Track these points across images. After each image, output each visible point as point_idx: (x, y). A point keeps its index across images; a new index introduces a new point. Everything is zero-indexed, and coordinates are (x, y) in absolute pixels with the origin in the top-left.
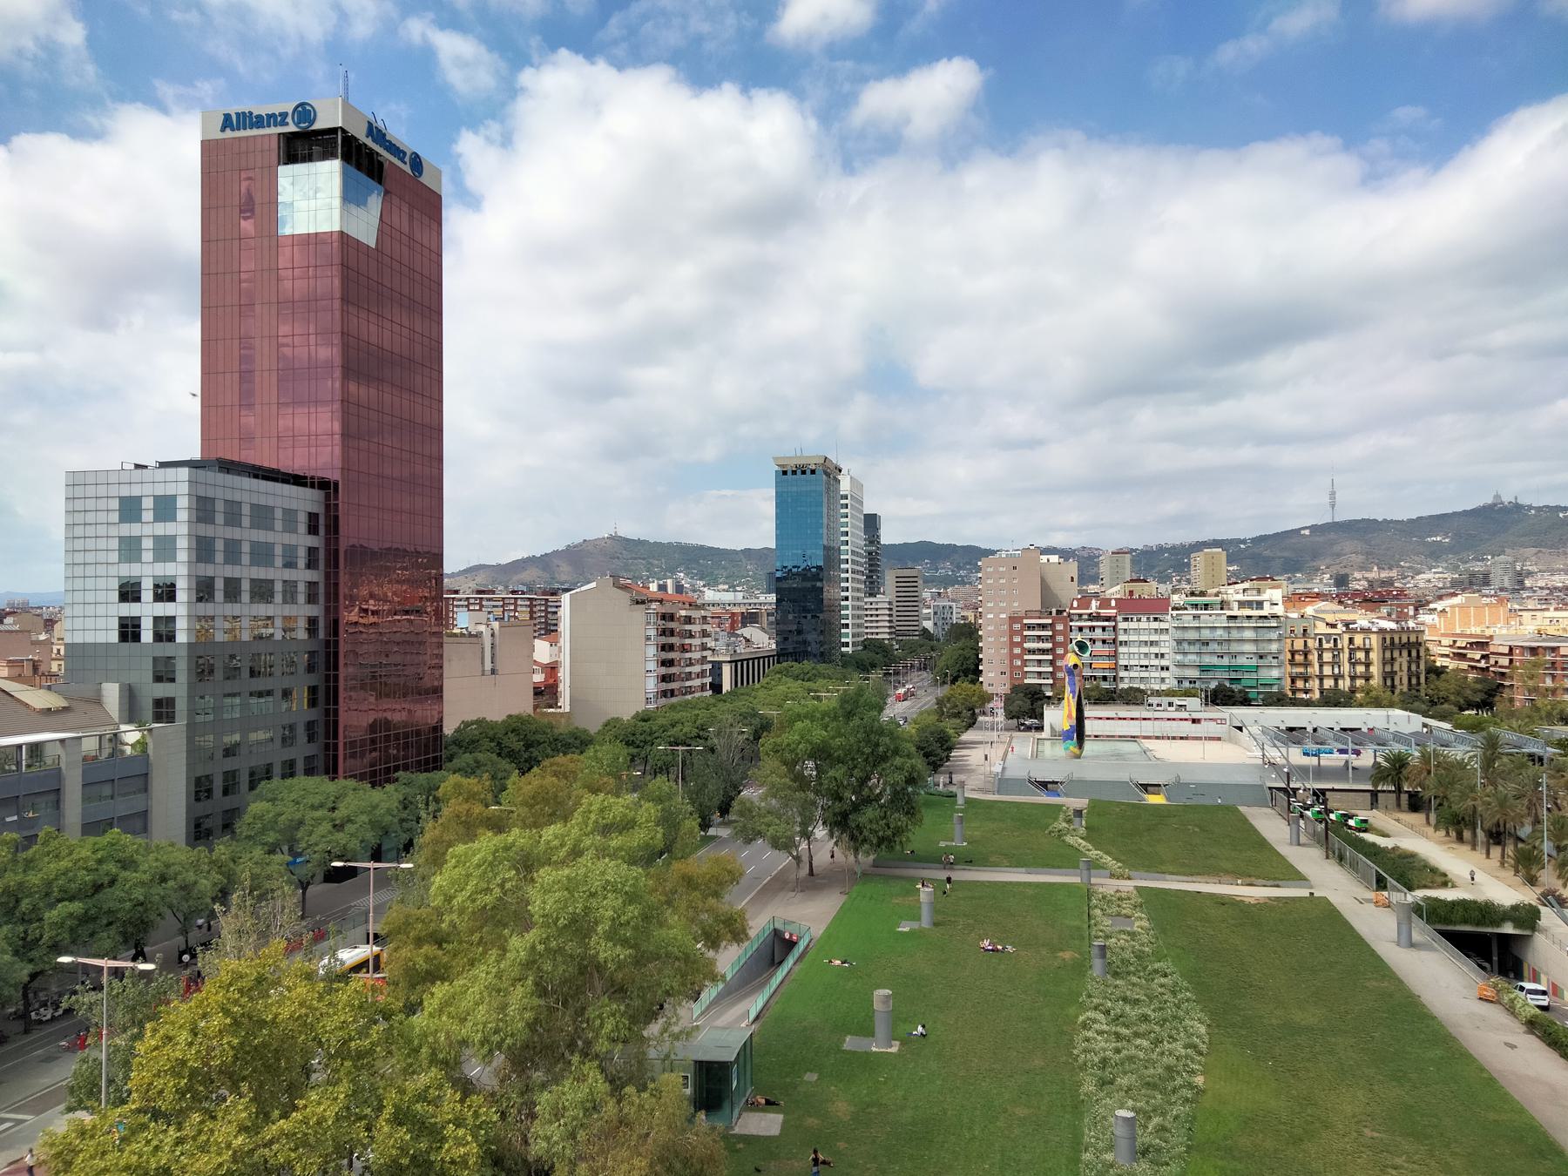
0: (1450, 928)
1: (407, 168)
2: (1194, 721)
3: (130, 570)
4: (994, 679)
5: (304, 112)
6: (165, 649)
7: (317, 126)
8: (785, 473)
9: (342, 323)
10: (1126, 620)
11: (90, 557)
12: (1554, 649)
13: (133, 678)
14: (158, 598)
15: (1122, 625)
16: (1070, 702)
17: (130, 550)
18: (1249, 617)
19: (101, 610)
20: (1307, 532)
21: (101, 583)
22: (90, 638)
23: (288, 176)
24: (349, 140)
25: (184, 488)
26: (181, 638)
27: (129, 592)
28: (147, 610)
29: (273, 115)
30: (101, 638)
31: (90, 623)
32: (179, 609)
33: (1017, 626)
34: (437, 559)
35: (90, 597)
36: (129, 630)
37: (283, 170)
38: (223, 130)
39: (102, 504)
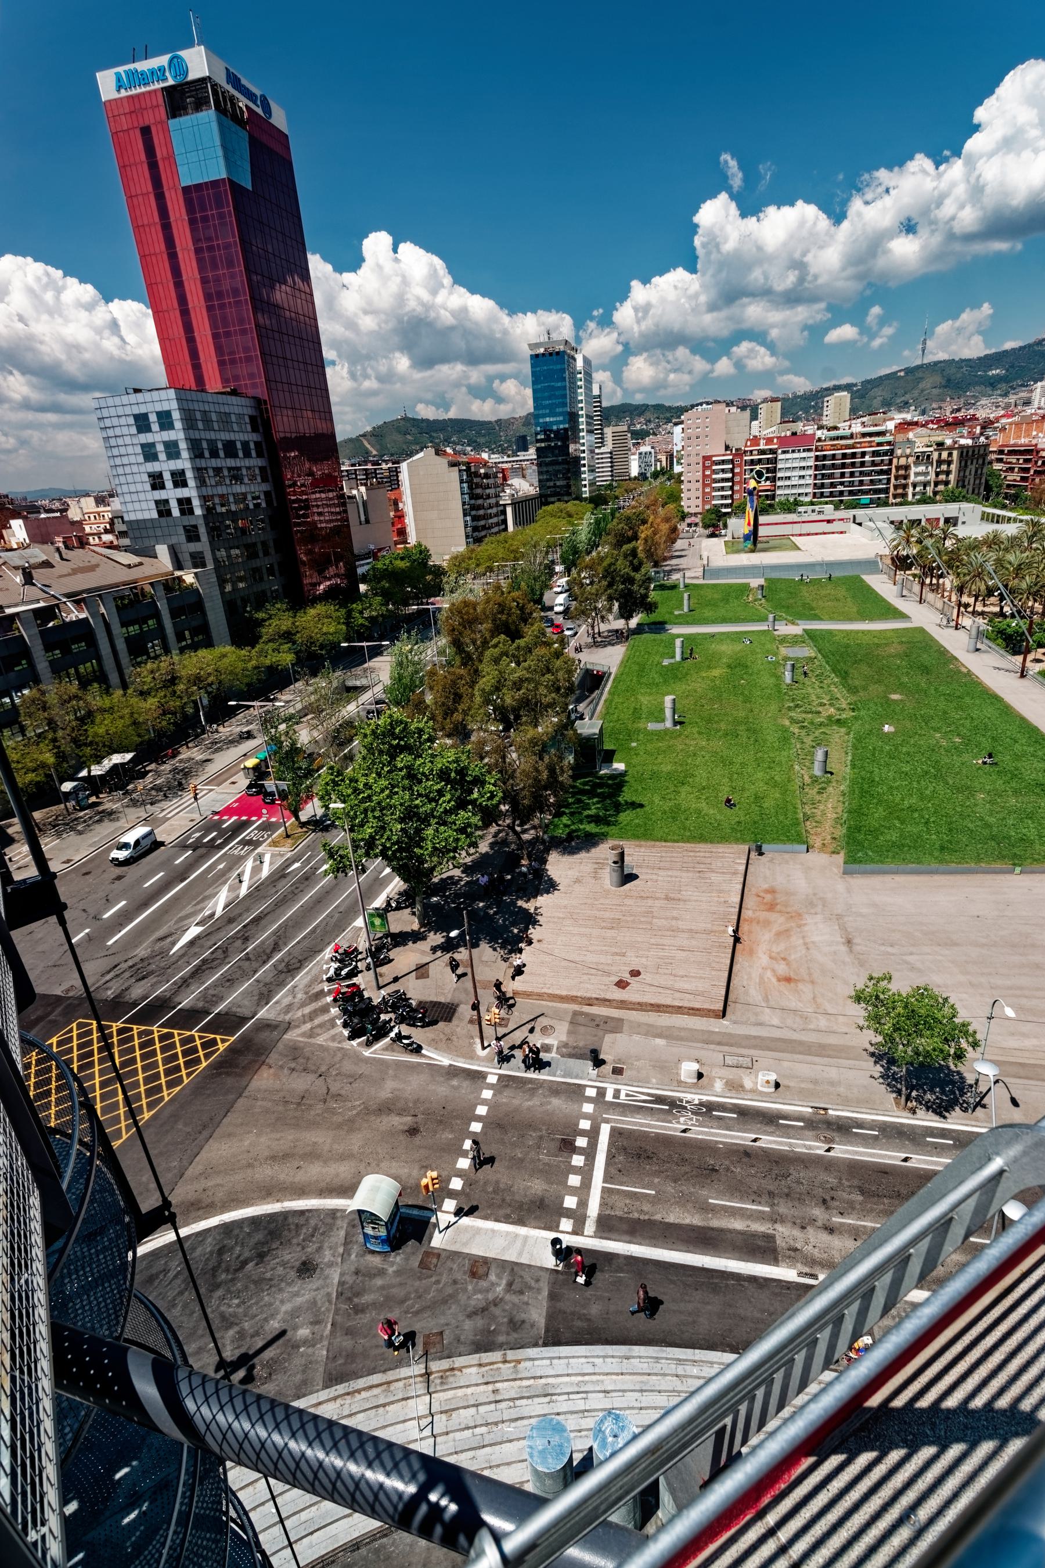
1: (259, 111)
2: (829, 521)
3: (154, 467)
4: (691, 501)
5: (177, 64)
10: (784, 452)
12: (825, 1109)
13: (174, 540)
15: (780, 457)
16: (750, 513)
17: (149, 453)
19: (142, 496)
20: (711, 344)
22: (140, 516)
25: (174, 405)
26: (198, 511)
27: (157, 482)
28: (172, 494)
30: (147, 516)
31: (137, 506)
32: (190, 491)
33: (708, 463)
34: (333, 436)
35: (133, 488)
37: (173, 123)
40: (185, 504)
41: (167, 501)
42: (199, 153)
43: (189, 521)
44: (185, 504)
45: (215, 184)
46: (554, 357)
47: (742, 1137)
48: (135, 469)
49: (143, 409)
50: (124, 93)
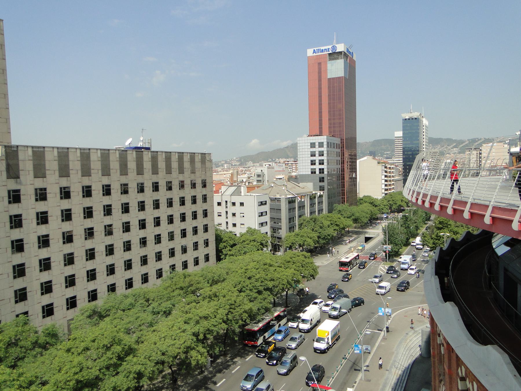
0: (431, 341)
5: (334, 47)
8: (406, 119)
9: (337, 106)
11: (304, 156)
14: (320, 164)
19: (307, 167)
21: (306, 153)
22: (304, 173)
23: (340, 140)
24: (345, 53)
25: (325, 140)
26: (326, 172)
27: (313, 163)
30: (307, 173)
31: (304, 170)
36: (313, 172)
39: (306, 144)
40: (321, 171)
42: (336, 69)
44: (321, 171)
45: (339, 78)
46: (414, 120)
47: (37, 150)
48: (306, 159)
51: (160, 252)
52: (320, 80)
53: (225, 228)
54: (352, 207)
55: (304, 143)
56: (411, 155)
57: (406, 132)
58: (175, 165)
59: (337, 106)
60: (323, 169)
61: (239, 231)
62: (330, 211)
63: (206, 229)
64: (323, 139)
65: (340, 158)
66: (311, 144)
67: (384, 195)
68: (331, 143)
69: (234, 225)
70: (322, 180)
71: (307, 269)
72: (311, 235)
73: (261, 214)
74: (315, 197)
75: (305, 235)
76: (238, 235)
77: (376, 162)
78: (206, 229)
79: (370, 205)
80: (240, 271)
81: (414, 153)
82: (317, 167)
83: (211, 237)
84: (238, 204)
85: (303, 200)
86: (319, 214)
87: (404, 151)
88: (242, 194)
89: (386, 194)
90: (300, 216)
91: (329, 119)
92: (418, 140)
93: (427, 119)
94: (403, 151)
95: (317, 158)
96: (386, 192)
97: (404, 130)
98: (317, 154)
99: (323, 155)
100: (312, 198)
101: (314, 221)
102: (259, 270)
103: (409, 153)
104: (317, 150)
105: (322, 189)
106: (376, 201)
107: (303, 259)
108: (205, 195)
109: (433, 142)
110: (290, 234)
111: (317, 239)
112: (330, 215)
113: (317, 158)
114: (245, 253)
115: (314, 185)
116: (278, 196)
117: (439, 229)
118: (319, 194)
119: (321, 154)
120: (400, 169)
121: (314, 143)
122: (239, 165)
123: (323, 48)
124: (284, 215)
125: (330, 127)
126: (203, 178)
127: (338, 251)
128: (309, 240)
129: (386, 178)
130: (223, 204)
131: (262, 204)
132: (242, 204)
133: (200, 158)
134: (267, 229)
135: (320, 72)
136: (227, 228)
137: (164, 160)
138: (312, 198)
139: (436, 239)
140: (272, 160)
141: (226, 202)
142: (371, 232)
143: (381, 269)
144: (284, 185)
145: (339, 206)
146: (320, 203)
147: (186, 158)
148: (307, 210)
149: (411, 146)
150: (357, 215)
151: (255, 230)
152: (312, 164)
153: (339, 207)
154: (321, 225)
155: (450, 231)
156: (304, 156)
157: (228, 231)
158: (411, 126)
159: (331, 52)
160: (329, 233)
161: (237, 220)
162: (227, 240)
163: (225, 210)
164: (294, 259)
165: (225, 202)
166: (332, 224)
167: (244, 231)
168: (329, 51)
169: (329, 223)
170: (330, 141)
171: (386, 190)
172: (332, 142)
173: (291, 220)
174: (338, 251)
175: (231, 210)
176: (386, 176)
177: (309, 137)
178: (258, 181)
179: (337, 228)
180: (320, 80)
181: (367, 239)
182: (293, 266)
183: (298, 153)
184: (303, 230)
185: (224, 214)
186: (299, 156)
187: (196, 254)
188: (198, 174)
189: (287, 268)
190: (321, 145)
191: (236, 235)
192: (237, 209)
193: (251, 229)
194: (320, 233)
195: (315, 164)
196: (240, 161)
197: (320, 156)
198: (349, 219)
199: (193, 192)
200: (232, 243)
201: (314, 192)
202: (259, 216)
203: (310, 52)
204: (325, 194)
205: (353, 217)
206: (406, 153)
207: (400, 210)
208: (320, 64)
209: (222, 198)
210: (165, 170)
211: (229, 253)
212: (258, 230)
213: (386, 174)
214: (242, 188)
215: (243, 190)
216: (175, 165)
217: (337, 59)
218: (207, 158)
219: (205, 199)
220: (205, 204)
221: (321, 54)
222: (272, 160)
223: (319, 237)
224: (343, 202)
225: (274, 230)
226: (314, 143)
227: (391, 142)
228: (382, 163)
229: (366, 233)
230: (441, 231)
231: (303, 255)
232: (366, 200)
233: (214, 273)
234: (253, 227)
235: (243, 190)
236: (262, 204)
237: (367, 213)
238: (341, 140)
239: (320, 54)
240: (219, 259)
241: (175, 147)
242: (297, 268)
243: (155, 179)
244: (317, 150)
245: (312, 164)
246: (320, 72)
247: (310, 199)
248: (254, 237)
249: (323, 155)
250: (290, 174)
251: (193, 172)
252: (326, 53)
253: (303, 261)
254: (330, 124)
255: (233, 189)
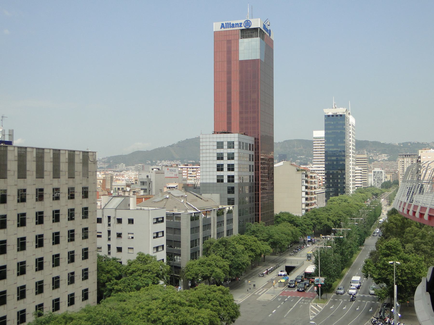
5: (248, 23)
6: (231, 185)
7: (251, 27)
8: (329, 116)
9: (245, 94)
11: (208, 159)
14: (229, 170)
18: (321, 173)
19: (211, 173)
21: (211, 155)
22: (208, 181)
23: (253, 139)
26: (236, 181)
27: (220, 168)
29: (238, 24)
30: (211, 181)
31: (208, 177)
34: (272, 139)
36: (220, 180)
38: (221, 28)
39: (211, 144)
40: (231, 179)
41: (223, 165)
42: (249, 49)
43: (231, 185)
44: (231, 179)
48: (211, 162)
49: (222, 140)
50: (223, 29)
51: (24, 287)
52: (229, 62)
53: (107, 254)
54: (269, 227)
55: (209, 142)
56: (335, 160)
57: (329, 132)
58: (48, 167)
59: (245, 94)
60: (233, 177)
61: (125, 258)
62: (241, 232)
63: (85, 255)
64: (234, 137)
65: (253, 163)
66: (218, 143)
67: (304, 212)
68: (243, 143)
69: (119, 250)
70: (231, 190)
71: (226, 308)
72: (221, 264)
73: (157, 235)
74: (223, 213)
75: (214, 263)
76: (125, 263)
77: (295, 169)
78: (85, 255)
79: (290, 225)
80: (141, 313)
81: (339, 158)
82: (226, 173)
83: (91, 264)
84: (125, 221)
85: (208, 217)
86: (227, 235)
87: (327, 155)
88: (131, 207)
89: (307, 210)
90: (205, 238)
91: (241, 113)
92: (344, 142)
93: (354, 116)
94: (325, 156)
95: (225, 162)
96: (307, 208)
97: (327, 128)
98: (225, 156)
99: (233, 158)
100: (220, 213)
101: (224, 245)
102: (166, 311)
103: (334, 158)
104: (225, 151)
105: (231, 202)
106: (298, 219)
107: (221, 295)
108: (86, 209)
109: (360, 145)
110: (193, 262)
111: (228, 269)
112: (243, 236)
113: (225, 162)
114: (138, 288)
115: (221, 197)
116: (176, 211)
117: (387, 255)
118: (227, 209)
119: (231, 157)
120: (320, 178)
121: (222, 143)
122: (108, 167)
123: (234, 22)
124: (186, 236)
125: (241, 123)
126: (84, 185)
127: (254, 285)
128: (218, 270)
129: (307, 190)
130: (105, 220)
131: (158, 221)
132: (131, 221)
133: (81, 157)
134: (162, 255)
135: (229, 52)
136: (109, 253)
137: (35, 159)
138: (220, 213)
139: (383, 269)
140: (152, 162)
141: (109, 217)
142: (292, 260)
143: (312, 308)
144: (182, 196)
145: (253, 225)
146: (230, 221)
147: (64, 158)
148: (214, 231)
149: (335, 149)
150: (276, 237)
151: (148, 256)
152: (218, 170)
153: (253, 226)
154: (234, 250)
155: (400, 259)
156: (208, 159)
157: (110, 257)
158: (335, 124)
159: (243, 28)
160: (245, 261)
161: (124, 243)
162: (111, 270)
163: (107, 228)
164: (209, 295)
165: (107, 218)
166: (246, 249)
167: (133, 257)
168: (241, 26)
169: (242, 247)
170: (242, 141)
171: (307, 205)
172: (245, 141)
173: (194, 243)
174: (254, 285)
175: (116, 228)
176: (306, 187)
177: (215, 135)
178: (145, 190)
179: (252, 254)
180: (229, 62)
181: (289, 270)
182: (210, 305)
183: (201, 155)
184: (210, 257)
185: (105, 235)
186: (201, 159)
187: (70, 289)
188: (78, 178)
189: (201, 308)
190: (231, 145)
191: (121, 263)
192: (124, 228)
193: (143, 254)
194: (232, 260)
195: (222, 170)
196: (108, 162)
197: (229, 159)
198: (266, 243)
199: (71, 204)
200: (117, 273)
201: (220, 207)
202: (154, 238)
203: (217, 27)
204: (235, 208)
205: (271, 240)
206: (329, 158)
207: (328, 231)
208: (229, 42)
209: (103, 212)
210: (35, 173)
211: (116, 287)
212: (152, 257)
213: (306, 184)
214: (131, 199)
215: (132, 201)
216: (48, 167)
217: (251, 37)
218: (91, 158)
219: (85, 213)
220: (85, 220)
221: (231, 29)
222: (152, 162)
223: (230, 266)
224: (257, 220)
225: (170, 256)
226: (222, 143)
227: (308, 144)
228: (302, 170)
229: (285, 261)
230: (389, 258)
231: (220, 290)
232: (284, 217)
233: (105, 315)
234: (146, 253)
235: (132, 201)
236: (158, 221)
237: (289, 235)
238: (255, 139)
239: (229, 29)
240: (100, 298)
241: (49, 142)
242: (214, 308)
243: (21, 184)
244: (225, 151)
245: (218, 170)
246: (229, 52)
247: (218, 215)
248: (149, 265)
249: (233, 158)
250: (184, 182)
251: (71, 176)
252: (237, 28)
253: (222, 298)
254: (241, 118)
255: (119, 200)
